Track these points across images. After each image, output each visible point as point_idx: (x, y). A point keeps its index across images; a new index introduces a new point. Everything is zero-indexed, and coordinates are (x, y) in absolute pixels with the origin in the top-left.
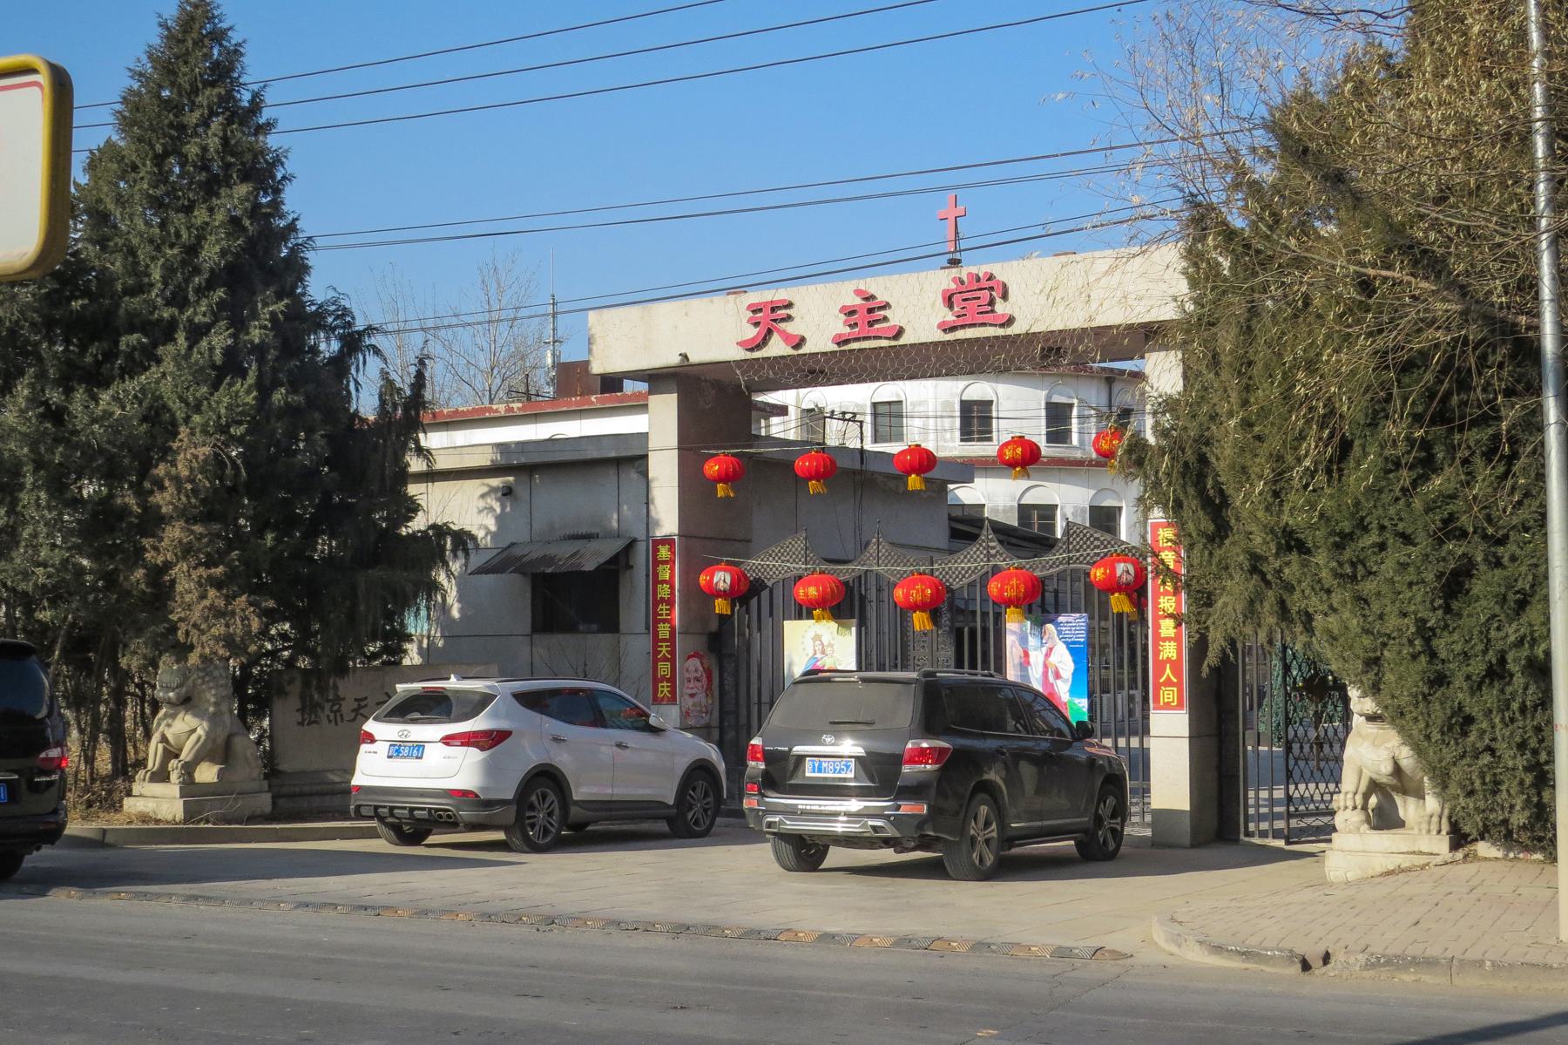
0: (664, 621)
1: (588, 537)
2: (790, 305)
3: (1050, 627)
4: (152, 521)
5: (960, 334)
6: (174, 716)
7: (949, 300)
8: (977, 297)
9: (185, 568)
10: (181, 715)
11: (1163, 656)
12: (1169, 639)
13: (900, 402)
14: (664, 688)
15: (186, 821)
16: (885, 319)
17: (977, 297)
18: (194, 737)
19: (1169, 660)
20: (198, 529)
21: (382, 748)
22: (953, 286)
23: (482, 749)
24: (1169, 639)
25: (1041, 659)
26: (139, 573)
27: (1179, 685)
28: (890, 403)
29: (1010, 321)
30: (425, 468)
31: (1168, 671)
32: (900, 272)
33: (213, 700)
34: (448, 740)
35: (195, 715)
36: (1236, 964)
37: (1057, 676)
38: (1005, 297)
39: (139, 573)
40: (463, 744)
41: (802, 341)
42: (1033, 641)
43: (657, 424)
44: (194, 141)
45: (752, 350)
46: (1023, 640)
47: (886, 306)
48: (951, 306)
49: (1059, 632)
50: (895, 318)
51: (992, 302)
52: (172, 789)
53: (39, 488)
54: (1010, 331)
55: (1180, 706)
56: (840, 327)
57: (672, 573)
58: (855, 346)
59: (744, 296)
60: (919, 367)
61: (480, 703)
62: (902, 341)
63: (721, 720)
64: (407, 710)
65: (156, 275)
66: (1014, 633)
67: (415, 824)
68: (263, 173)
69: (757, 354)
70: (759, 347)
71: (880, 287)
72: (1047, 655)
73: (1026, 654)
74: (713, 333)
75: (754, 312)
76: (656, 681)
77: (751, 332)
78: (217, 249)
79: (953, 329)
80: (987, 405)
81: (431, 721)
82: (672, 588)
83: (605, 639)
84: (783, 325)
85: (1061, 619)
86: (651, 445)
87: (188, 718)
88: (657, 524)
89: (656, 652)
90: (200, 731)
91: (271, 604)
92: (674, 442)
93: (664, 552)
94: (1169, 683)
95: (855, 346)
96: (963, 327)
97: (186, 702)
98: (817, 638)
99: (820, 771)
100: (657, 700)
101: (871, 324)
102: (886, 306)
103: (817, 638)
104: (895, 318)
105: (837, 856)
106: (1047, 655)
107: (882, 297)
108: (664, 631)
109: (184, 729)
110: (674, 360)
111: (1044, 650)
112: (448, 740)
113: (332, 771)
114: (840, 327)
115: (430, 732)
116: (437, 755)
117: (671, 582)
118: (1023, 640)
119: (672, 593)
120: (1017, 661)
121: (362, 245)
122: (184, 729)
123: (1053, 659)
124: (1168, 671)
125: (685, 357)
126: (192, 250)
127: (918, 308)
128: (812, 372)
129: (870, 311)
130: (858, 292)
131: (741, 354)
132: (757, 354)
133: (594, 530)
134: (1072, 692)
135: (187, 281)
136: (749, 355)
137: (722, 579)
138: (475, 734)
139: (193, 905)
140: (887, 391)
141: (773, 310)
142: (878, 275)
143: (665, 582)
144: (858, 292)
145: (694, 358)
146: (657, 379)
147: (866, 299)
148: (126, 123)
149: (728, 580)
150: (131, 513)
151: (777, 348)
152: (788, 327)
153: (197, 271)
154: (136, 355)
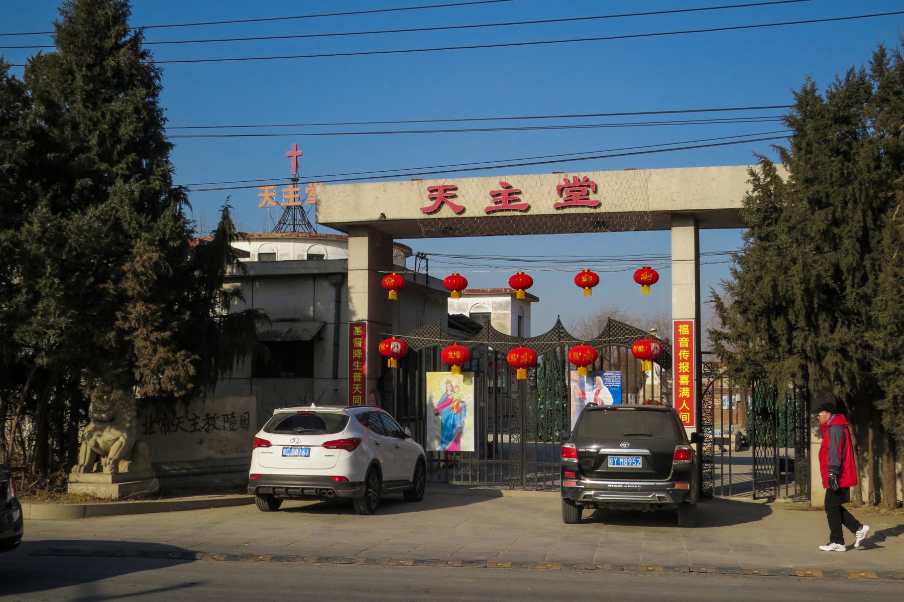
0: (358, 371)
1: (293, 320)
2: (456, 189)
3: (599, 378)
4: (122, 299)
5: (567, 211)
6: (102, 430)
7: (561, 190)
8: (578, 191)
9: (145, 331)
10: (108, 429)
11: (682, 395)
12: (685, 386)
13: (274, 254)
15: (121, 498)
16: (519, 200)
17: (578, 191)
18: (117, 444)
19: (685, 398)
20: (153, 307)
21: (276, 450)
22: (563, 183)
23: (349, 451)
24: (685, 386)
26: (112, 335)
27: (691, 411)
28: (268, 254)
29: (599, 205)
31: (684, 404)
32: (528, 173)
33: (129, 419)
34: (327, 445)
35: (117, 429)
38: (595, 192)
39: (112, 335)
40: (338, 448)
41: (463, 210)
42: (587, 387)
43: (357, 253)
44: (106, 60)
45: (558, 209)
46: (582, 385)
47: (519, 193)
48: (561, 195)
49: (604, 381)
50: (524, 199)
51: (588, 194)
52: (106, 476)
53: (55, 276)
54: (598, 211)
56: (489, 202)
57: (364, 344)
59: (424, 182)
60: (533, 230)
61: (339, 424)
62: (529, 213)
64: (287, 426)
65: (94, 141)
66: (575, 381)
67: (273, 495)
68: (148, 80)
69: (432, 216)
70: (435, 212)
71: (515, 181)
72: (597, 394)
73: (584, 393)
74: (404, 201)
75: (431, 191)
77: (430, 204)
78: (131, 127)
79: (563, 207)
81: (313, 433)
82: (363, 352)
84: (450, 200)
85: (605, 374)
86: (350, 267)
87: (113, 430)
88: (353, 313)
89: (351, 390)
90: (122, 439)
91: (197, 357)
92: (366, 266)
93: (358, 331)
96: (570, 207)
97: (112, 421)
98: (449, 382)
99: (618, 464)
101: (510, 202)
102: (519, 193)
103: (449, 382)
104: (524, 199)
105: (286, 504)
106: (597, 394)
107: (516, 187)
108: (357, 377)
109: (113, 439)
110: (376, 216)
111: (595, 391)
112: (327, 445)
113: (165, 463)
114: (489, 202)
115: (316, 440)
116: (318, 453)
118: (582, 385)
119: (364, 355)
120: (577, 397)
122: (113, 439)
123: (600, 396)
124: (684, 404)
125: (383, 215)
126: (115, 126)
127: (541, 194)
128: (598, 223)
129: (509, 195)
130: (502, 184)
131: (554, 211)
132: (432, 216)
135: (113, 146)
136: (427, 216)
137: (396, 347)
138: (345, 441)
139: (420, 566)
141: (445, 190)
142: (469, 176)
143: (359, 348)
144: (502, 184)
145: (389, 216)
146: (352, 229)
147: (506, 188)
149: (399, 346)
150: (108, 293)
151: (446, 212)
152: (455, 201)
153: (119, 141)
154: (86, 192)
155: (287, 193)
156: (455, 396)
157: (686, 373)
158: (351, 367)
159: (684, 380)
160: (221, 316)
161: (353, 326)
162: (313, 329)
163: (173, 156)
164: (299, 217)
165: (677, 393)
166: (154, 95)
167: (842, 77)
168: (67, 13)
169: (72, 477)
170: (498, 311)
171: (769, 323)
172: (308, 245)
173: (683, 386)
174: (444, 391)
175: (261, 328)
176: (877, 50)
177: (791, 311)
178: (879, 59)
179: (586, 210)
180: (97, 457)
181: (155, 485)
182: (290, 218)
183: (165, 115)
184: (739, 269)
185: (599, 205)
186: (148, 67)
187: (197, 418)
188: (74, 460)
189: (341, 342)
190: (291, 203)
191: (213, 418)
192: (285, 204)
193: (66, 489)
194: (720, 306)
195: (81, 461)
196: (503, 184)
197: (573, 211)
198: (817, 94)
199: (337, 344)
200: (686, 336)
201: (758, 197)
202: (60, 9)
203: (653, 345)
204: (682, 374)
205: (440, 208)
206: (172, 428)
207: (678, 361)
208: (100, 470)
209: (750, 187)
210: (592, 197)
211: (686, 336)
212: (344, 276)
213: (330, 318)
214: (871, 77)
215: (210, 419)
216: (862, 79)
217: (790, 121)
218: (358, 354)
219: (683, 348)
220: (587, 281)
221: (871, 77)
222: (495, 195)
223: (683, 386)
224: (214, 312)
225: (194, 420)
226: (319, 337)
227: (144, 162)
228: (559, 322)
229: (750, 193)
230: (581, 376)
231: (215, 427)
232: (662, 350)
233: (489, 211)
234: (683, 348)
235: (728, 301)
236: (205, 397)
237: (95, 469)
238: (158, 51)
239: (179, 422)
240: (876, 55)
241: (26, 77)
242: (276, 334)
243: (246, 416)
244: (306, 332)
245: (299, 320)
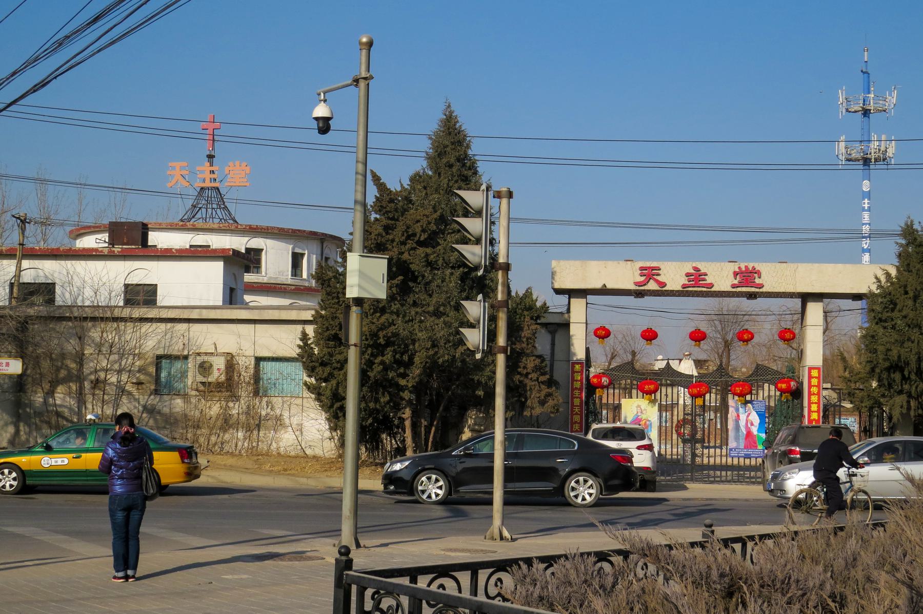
7: (736, 274)
11: (812, 418)
25: (745, 418)
34: (639, 448)
36: (468, 554)
37: (752, 424)
38: (760, 277)
46: (737, 410)
47: (706, 275)
50: (709, 280)
54: (761, 290)
56: (684, 281)
62: (713, 289)
72: (748, 416)
73: (738, 416)
77: (643, 279)
80: (258, 251)
81: (629, 440)
88: (574, 354)
89: (572, 411)
93: (577, 367)
98: (639, 406)
102: (706, 275)
103: (639, 406)
104: (709, 280)
106: (748, 416)
108: (577, 402)
112: (639, 448)
114: (684, 281)
117: (581, 380)
118: (737, 410)
123: (750, 418)
125: (605, 285)
134: (758, 431)
136: (638, 288)
140: (256, 242)
151: (652, 286)
155: (202, 172)
156: (644, 417)
161: (574, 364)
165: (809, 416)
171: (889, 375)
172: (247, 239)
177: (906, 370)
190: (208, 184)
192: (199, 184)
196: (696, 269)
198: (915, 227)
203: (792, 383)
210: (757, 281)
212: (566, 325)
218: (577, 385)
222: (688, 275)
232: (797, 388)
233: (684, 286)
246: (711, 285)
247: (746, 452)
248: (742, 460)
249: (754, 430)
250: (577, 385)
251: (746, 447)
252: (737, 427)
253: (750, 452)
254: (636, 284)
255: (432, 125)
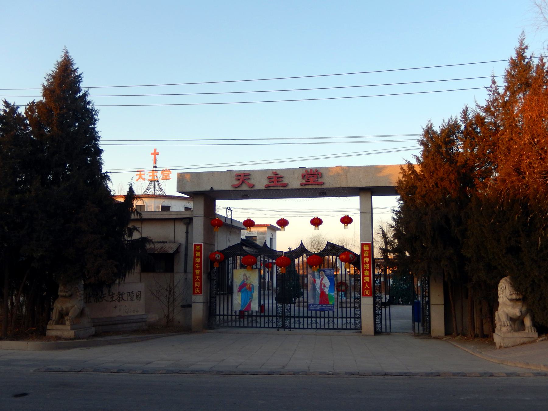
5: (307, 187)
13: (170, 207)
14: (197, 290)
19: (367, 282)
27: (370, 289)
30: (139, 218)
37: (325, 286)
46: (314, 276)
54: (323, 187)
55: (370, 295)
58: (272, 188)
63: (210, 300)
69: (238, 189)
70: (239, 186)
72: (321, 281)
73: (315, 281)
76: (195, 288)
77: (236, 183)
79: (305, 185)
83: (168, 275)
93: (198, 248)
94: (367, 288)
95: (272, 188)
100: (195, 294)
102: (282, 177)
106: (321, 281)
110: (208, 188)
121: (339, 143)
123: (323, 282)
125: (212, 188)
132: (238, 189)
133: (165, 240)
148: (44, 95)
151: (245, 187)
156: (248, 282)
157: (368, 270)
158: (195, 267)
159: (367, 273)
160: (128, 241)
162: (174, 247)
163: (103, 156)
164: (157, 186)
166: (95, 124)
167: (447, 121)
168: (49, 80)
169: (49, 327)
170: (260, 236)
173: (366, 276)
174: (243, 279)
175: (148, 246)
176: (464, 108)
178: (465, 112)
179: (317, 187)
180: (62, 316)
181: (93, 330)
182: (152, 187)
183: (100, 134)
184: (395, 217)
185: (322, 184)
186: (92, 109)
187: (113, 294)
188: (49, 318)
189: (189, 254)
191: (122, 294)
193: (45, 334)
194: (384, 236)
195: (54, 318)
197: (310, 187)
199: (186, 255)
200: (367, 251)
201: (405, 181)
202: (494, 82)
203: (351, 255)
204: (366, 270)
205: (241, 184)
206: (100, 300)
207: (369, 263)
208: (63, 323)
209: (401, 176)
210: (320, 180)
211: (367, 251)
213: (183, 240)
214: (461, 120)
215: (120, 294)
216: (456, 122)
217: (422, 143)
218: (198, 260)
219: (366, 257)
220: (316, 222)
221: (461, 120)
223: (366, 276)
224: (124, 238)
225: (112, 295)
226: (177, 251)
227: (89, 159)
228: (302, 243)
229: (401, 179)
230: (314, 272)
231: (123, 299)
233: (267, 186)
234: (366, 257)
235: (390, 234)
236: (119, 283)
237: (60, 322)
238: (96, 100)
239: (104, 297)
240: (464, 110)
241: (26, 113)
242: (154, 249)
243: (139, 293)
244: (171, 248)
245: (167, 242)
246: (286, 185)
247: (320, 306)
248: (318, 312)
249: (326, 291)
250: (198, 260)
251: (320, 303)
252: (314, 288)
253: (324, 306)
254: (233, 186)
255: (51, 68)
